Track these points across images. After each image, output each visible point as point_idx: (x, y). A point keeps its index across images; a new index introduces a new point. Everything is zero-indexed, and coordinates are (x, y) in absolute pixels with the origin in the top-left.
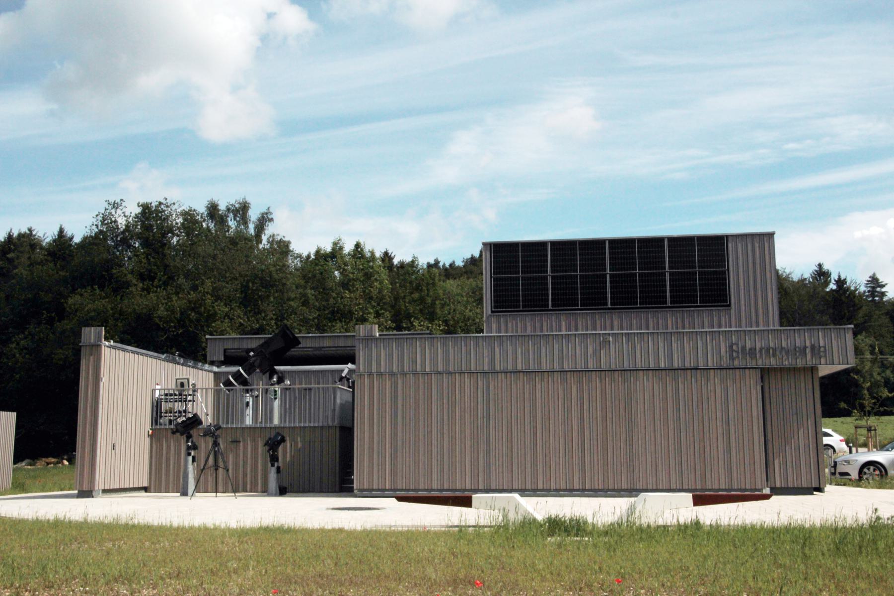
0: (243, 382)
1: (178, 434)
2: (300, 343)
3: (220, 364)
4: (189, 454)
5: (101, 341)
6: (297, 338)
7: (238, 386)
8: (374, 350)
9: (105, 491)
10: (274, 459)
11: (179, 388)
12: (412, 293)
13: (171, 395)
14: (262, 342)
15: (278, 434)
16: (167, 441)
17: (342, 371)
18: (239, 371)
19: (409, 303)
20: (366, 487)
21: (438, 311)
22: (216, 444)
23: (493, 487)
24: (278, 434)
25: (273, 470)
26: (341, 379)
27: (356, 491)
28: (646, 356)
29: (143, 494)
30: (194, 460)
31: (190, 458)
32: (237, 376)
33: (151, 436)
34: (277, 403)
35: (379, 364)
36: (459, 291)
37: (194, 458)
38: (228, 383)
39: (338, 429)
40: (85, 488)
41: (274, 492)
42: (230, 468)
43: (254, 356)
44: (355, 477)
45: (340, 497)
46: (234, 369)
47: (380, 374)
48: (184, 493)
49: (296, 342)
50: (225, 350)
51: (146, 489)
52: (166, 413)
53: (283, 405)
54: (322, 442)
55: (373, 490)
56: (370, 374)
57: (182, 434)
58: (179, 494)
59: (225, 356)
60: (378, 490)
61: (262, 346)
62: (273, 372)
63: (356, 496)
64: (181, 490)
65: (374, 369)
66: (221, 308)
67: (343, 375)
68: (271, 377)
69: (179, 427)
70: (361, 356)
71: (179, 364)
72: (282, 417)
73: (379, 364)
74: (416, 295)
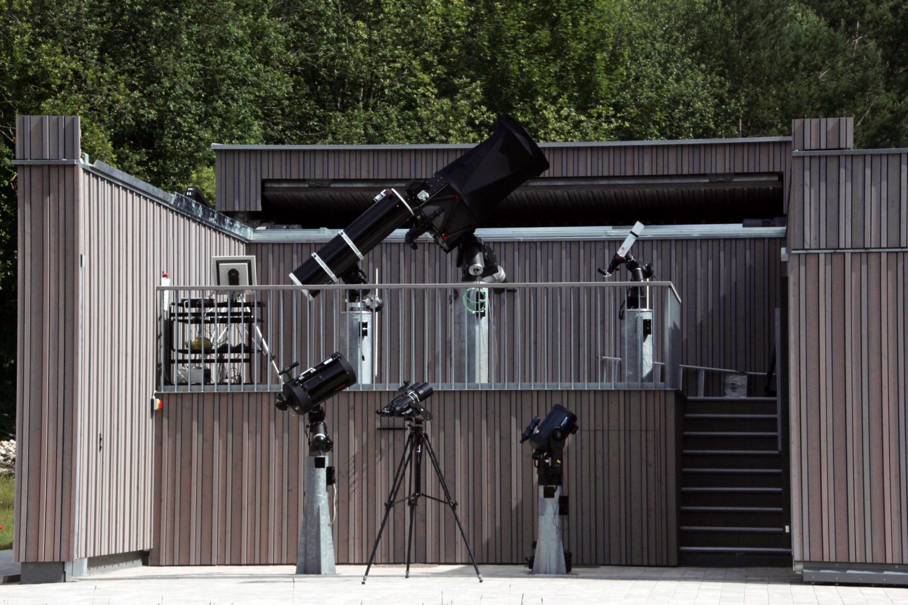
0: (351, 273)
1: (291, 413)
2: (546, 166)
3: (252, 219)
4: (320, 463)
5: (74, 156)
6: (539, 152)
7: (339, 285)
8: (846, 189)
9: (96, 562)
10: (551, 478)
11: (224, 284)
12: (531, 29)
13: (210, 303)
14: (442, 163)
15: (559, 409)
16: (201, 429)
17: (621, 241)
18: (339, 237)
19: (529, 55)
20: (829, 554)
21: (603, 81)
22: (418, 437)
23: (634, 563)
24: (559, 409)
25: (550, 507)
26: (616, 262)
27: (798, 568)
28: (894, 211)
29: (138, 569)
30: (330, 481)
31: (322, 473)
32: (336, 253)
33: (158, 415)
34: (483, 327)
35: (859, 227)
36: (647, 26)
37: (330, 472)
38: (310, 274)
39: (671, 399)
40: (46, 555)
41: (554, 566)
42: (460, 497)
43: (429, 202)
44: (795, 529)
45: (746, 580)
46: (326, 234)
47: (864, 253)
48: (310, 566)
49: (536, 162)
50: (264, 182)
51: (145, 557)
52: (184, 352)
53: (496, 334)
54: (628, 431)
55: (884, 566)
56: (836, 252)
57: (302, 412)
58: (293, 569)
59: (264, 200)
60: (864, 565)
61: (447, 171)
62: (467, 247)
63: (800, 580)
64: (301, 559)
65: (846, 240)
66: (57, 61)
67: (622, 253)
68: (465, 260)
69: (298, 391)
70: (807, 200)
71: (193, 218)
72: (497, 371)
73: (859, 227)
74: (543, 35)
